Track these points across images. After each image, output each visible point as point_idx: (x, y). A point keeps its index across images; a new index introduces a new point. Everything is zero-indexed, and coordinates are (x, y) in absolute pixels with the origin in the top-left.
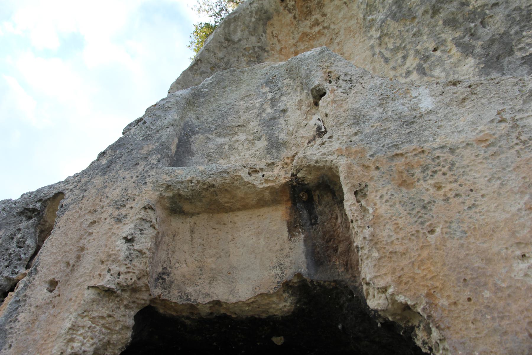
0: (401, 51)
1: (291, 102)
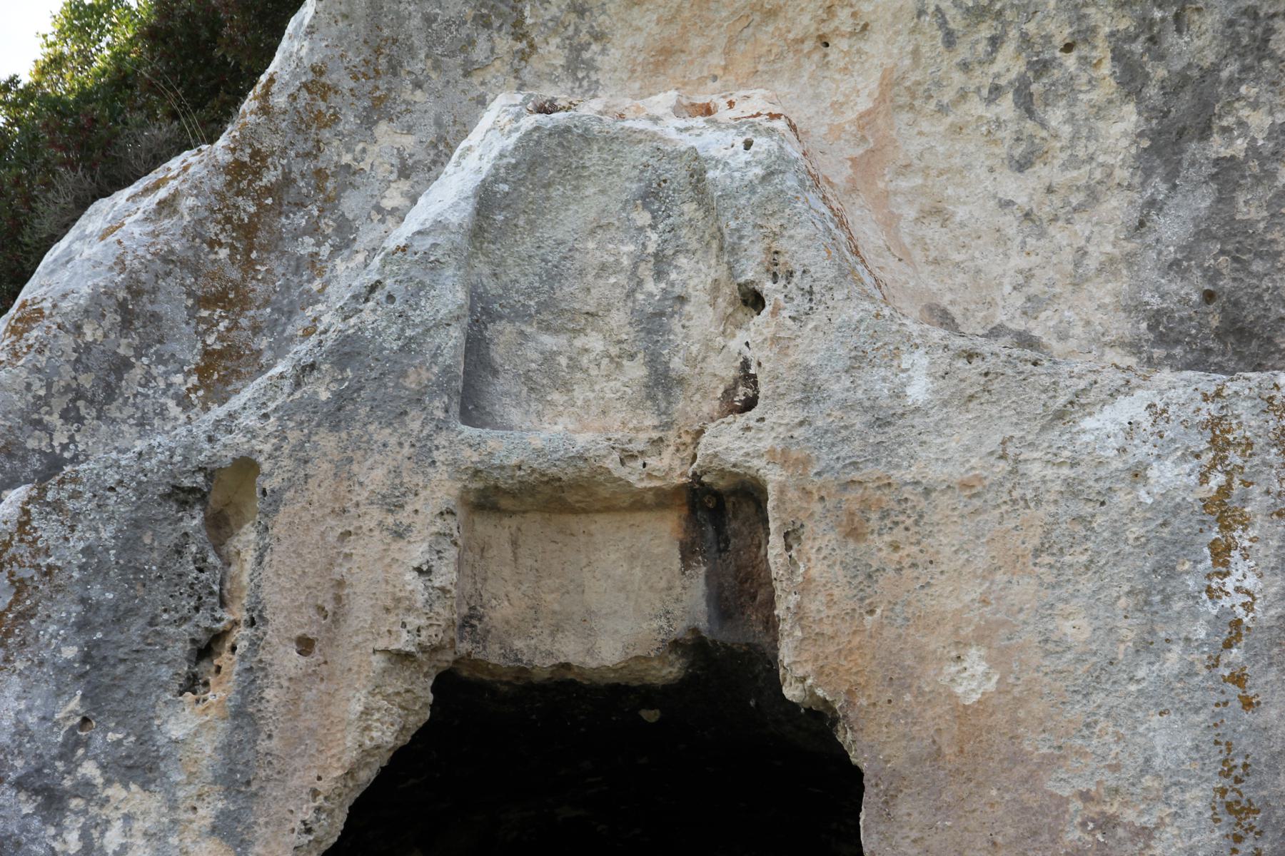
0: (990, 21)
1: (696, 281)
